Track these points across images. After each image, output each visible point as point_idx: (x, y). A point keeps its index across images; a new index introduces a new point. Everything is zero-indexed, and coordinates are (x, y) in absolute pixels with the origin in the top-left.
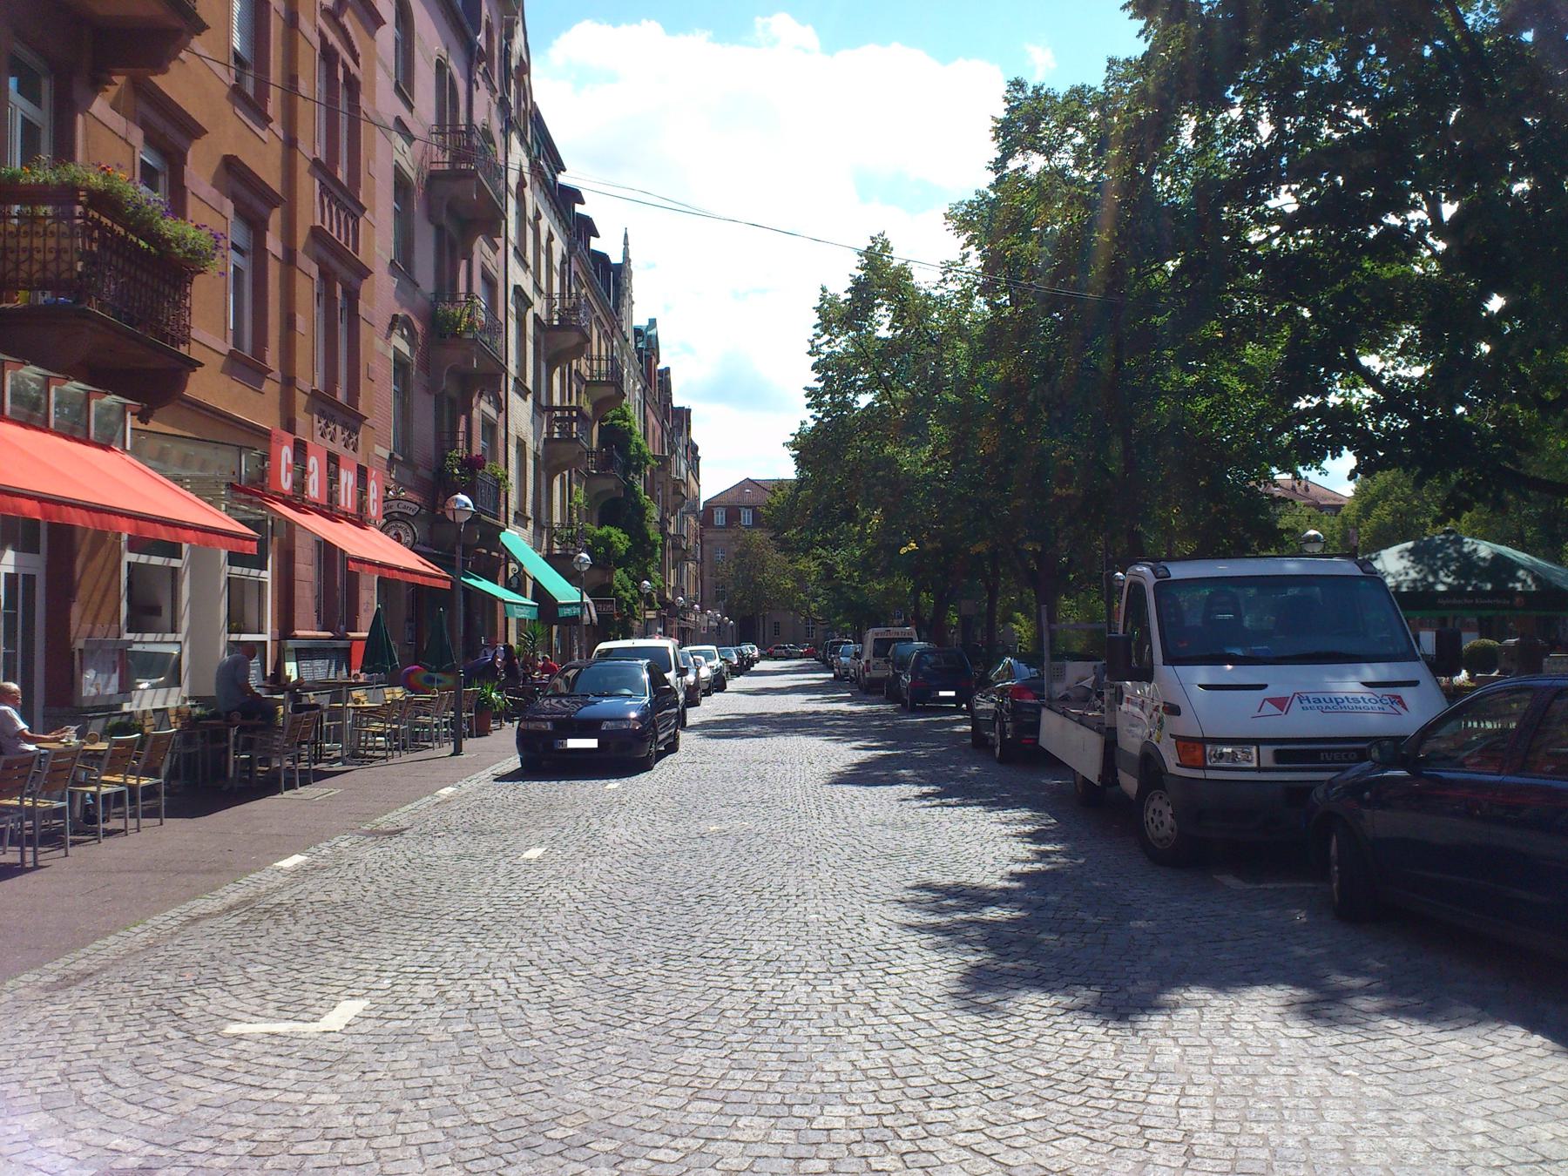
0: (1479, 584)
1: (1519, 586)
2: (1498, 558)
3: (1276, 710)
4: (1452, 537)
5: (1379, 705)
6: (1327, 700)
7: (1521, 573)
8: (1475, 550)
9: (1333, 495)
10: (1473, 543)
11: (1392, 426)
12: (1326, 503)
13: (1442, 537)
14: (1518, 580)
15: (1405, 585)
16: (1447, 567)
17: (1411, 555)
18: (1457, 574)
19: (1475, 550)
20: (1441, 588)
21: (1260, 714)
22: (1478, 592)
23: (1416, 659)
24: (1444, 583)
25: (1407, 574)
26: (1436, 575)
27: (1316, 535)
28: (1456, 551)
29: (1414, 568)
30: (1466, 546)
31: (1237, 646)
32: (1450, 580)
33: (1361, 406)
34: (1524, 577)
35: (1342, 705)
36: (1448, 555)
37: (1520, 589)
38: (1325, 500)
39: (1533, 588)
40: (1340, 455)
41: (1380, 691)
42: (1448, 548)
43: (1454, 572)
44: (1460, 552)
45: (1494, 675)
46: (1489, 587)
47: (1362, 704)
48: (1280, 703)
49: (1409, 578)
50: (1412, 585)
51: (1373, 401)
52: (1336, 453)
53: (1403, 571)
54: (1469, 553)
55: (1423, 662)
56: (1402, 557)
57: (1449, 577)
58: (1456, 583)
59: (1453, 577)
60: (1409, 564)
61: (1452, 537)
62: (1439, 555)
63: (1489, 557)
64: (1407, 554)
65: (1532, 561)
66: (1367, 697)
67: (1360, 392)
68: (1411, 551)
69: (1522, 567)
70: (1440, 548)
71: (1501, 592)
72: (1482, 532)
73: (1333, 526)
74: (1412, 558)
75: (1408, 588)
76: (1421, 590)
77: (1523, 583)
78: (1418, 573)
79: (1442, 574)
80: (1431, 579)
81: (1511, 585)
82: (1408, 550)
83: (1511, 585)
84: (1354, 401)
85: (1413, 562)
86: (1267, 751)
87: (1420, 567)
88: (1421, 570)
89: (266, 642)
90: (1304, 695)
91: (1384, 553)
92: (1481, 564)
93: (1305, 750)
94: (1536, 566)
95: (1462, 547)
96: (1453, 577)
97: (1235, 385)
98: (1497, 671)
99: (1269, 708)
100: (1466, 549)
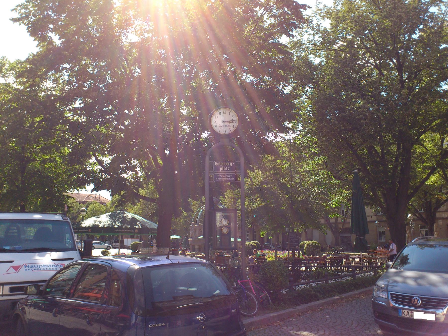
0: (127, 226)
1: (137, 227)
2: (133, 218)
3: (14, 271)
4: (122, 212)
5: (56, 267)
6: (36, 266)
7: (138, 223)
8: (127, 216)
9: (106, 200)
10: (127, 214)
11: (105, 177)
12: (104, 202)
13: (119, 211)
14: (137, 225)
15: (106, 225)
16: (119, 220)
17: (109, 216)
18: (121, 223)
19: (127, 216)
20: (116, 226)
21: (7, 273)
22: (126, 228)
23: (76, 250)
24: (117, 225)
25: (107, 222)
26: (115, 223)
27: (84, 210)
28: (122, 216)
29: (110, 220)
30: (125, 214)
31: (6, 245)
32: (119, 224)
33: (97, 171)
34: (138, 224)
35: (41, 268)
36: (120, 217)
37: (137, 227)
38: (104, 201)
39: (140, 227)
40: (90, 185)
41: (57, 262)
42: (120, 215)
43: (120, 222)
44: (123, 216)
45: (136, 252)
46: (129, 227)
47: (49, 267)
48: (17, 268)
49: (108, 223)
50: (108, 226)
51: (100, 170)
52: (89, 184)
53: (106, 221)
54: (126, 216)
55: (78, 251)
56: (107, 217)
57: (119, 223)
58: (120, 225)
59: (120, 223)
60: (109, 219)
61: (122, 212)
62: (117, 217)
63: (130, 218)
64: (108, 216)
65: (142, 219)
66: (51, 264)
67: (97, 166)
68: (110, 215)
69: (138, 221)
70: (118, 215)
71: (132, 228)
72: (142, 212)
73: (104, 208)
74: (110, 217)
75: (107, 226)
76: (110, 227)
77: (138, 226)
78: (111, 222)
79: (117, 222)
80: (114, 224)
81: (135, 226)
82: (109, 215)
83: (135, 226)
84: (95, 169)
85: (110, 219)
86: (7, 288)
87: (111, 220)
88: (111, 221)
89: (421, 228)
90: (27, 265)
91: (102, 215)
92: (128, 220)
93: (14, 287)
94: (143, 221)
95: (124, 215)
96: (120, 223)
97: (59, 160)
98: (137, 251)
99: (12, 270)
100: (125, 216)
